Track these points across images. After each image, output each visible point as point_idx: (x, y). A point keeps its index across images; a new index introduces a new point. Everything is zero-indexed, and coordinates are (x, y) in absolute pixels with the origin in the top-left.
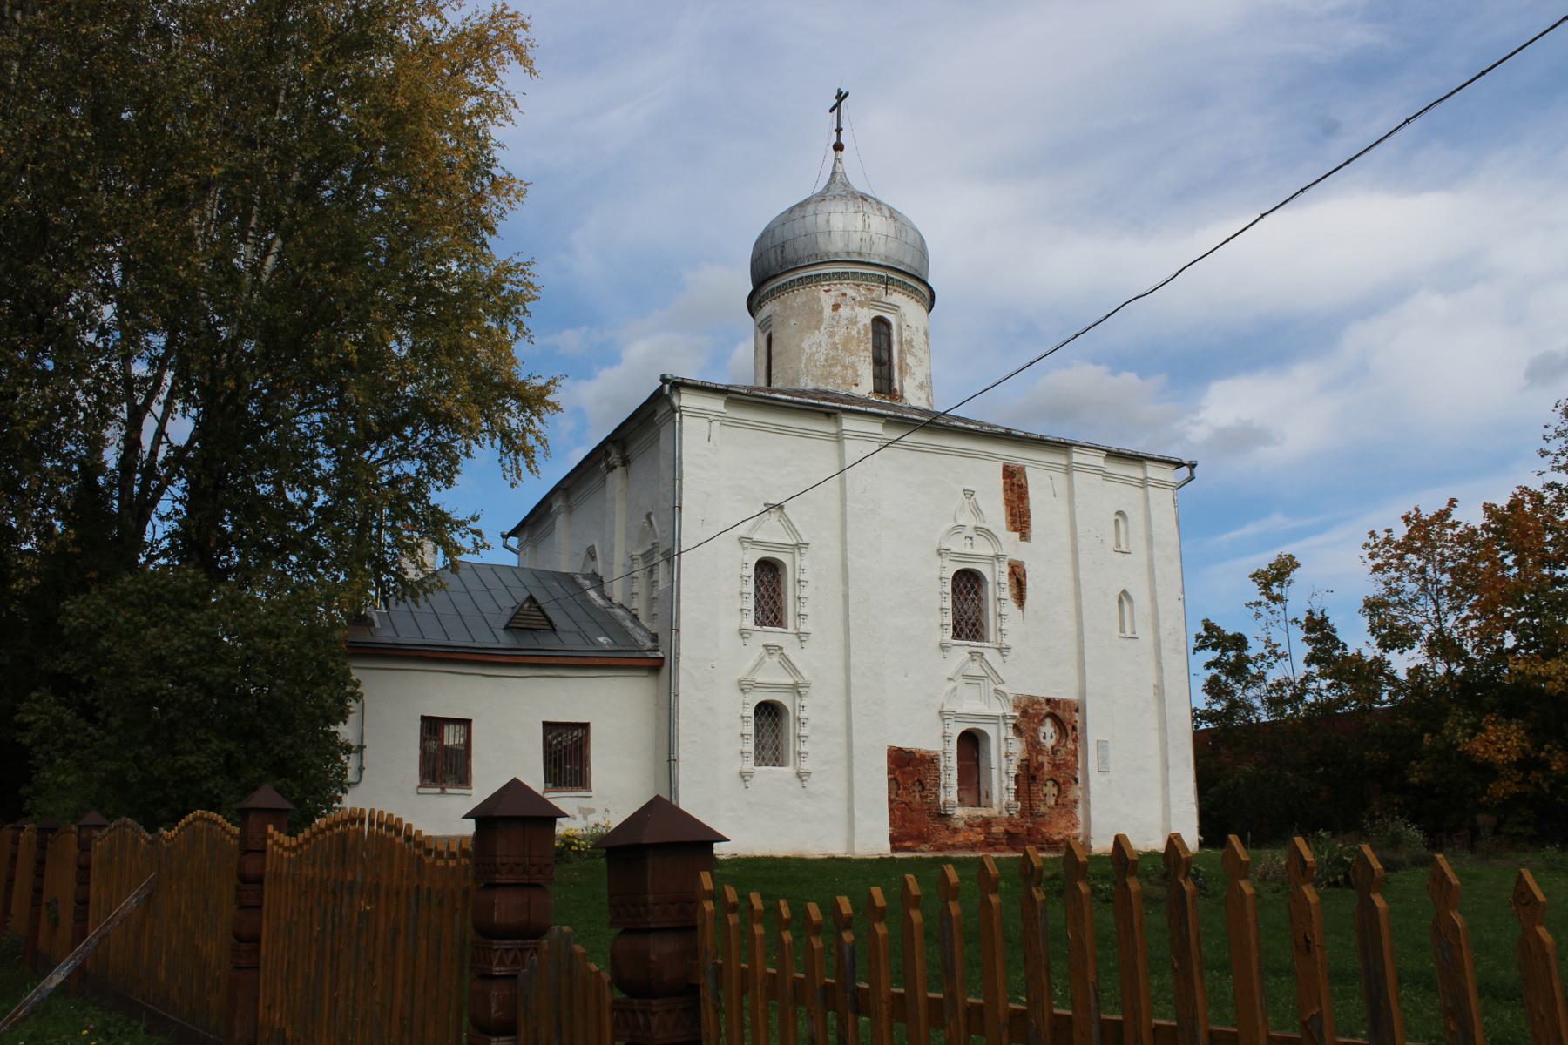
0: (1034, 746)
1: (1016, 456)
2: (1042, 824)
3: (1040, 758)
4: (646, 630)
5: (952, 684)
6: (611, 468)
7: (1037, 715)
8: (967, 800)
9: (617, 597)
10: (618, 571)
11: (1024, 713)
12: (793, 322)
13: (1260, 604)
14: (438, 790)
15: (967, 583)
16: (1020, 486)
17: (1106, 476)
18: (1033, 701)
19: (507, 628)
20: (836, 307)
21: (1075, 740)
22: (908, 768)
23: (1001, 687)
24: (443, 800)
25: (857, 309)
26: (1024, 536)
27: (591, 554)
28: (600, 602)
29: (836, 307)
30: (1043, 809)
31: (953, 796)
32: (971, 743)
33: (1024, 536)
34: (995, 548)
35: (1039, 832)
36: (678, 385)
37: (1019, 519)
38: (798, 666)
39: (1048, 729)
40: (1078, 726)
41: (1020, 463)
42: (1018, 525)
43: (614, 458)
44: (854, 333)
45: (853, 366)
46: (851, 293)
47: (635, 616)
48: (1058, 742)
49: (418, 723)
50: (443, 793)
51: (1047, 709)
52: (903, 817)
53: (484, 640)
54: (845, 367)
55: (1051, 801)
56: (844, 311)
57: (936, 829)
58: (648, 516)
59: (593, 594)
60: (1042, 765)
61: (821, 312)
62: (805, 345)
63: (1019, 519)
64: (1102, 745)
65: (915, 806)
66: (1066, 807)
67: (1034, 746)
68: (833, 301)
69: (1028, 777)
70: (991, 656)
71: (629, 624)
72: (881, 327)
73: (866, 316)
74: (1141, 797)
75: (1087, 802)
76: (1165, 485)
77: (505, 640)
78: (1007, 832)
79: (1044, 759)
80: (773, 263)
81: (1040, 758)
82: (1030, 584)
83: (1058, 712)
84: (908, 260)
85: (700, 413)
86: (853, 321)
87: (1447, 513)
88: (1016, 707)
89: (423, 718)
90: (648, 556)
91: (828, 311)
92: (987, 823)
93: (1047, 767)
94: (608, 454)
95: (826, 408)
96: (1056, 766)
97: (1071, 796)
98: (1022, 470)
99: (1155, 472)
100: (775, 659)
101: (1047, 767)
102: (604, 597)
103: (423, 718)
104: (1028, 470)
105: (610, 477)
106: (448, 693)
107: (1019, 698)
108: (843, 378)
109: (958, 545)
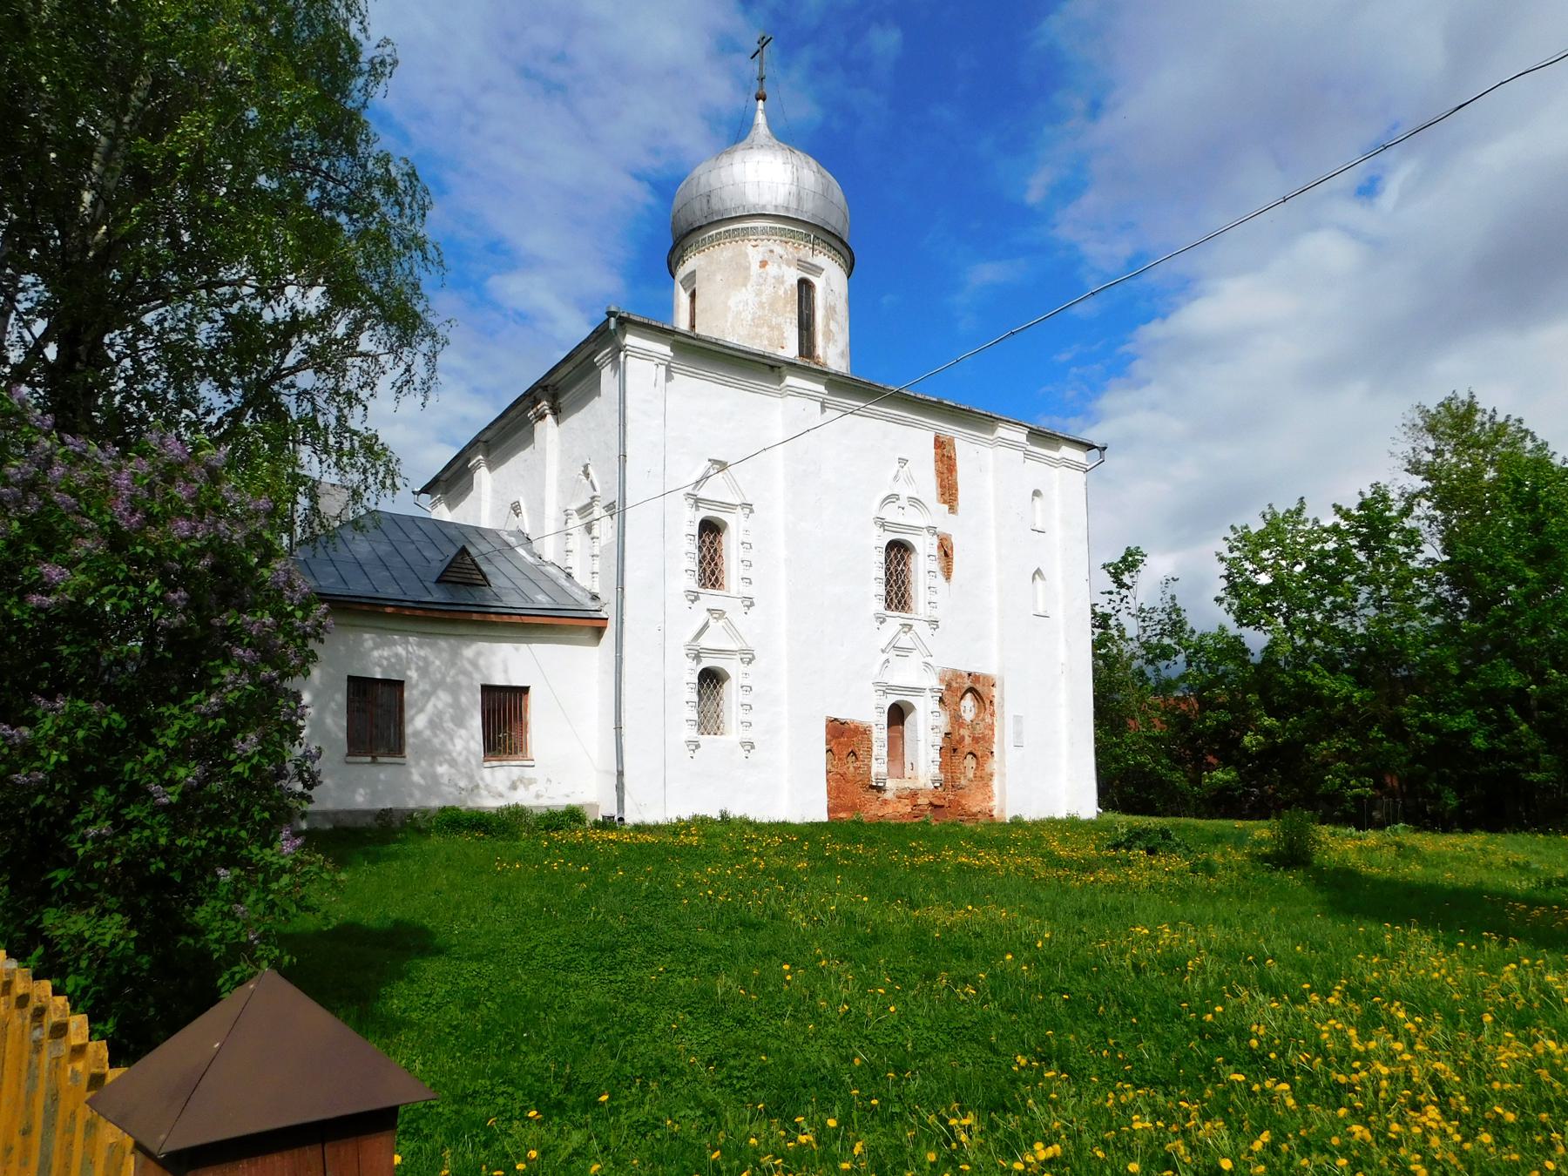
0: (956, 719)
1: (949, 430)
2: (962, 796)
3: (962, 732)
4: (584, 590)
5: (885, 656)
6: (542, 417)
7: (959, 689)
8: (893, 771)
9: (549, 556)
10: (551, 523)
11: (949, 686)
12: (719, 277)
13: (1111, 593)
14: (369, 759)
15: (898, 550)
16: (950, 458)
17: (1028, 455)
18: (957, 675)
19: (439, 581)
20: (763, 264)
21: (992, 715)
22: (844, 738)
23: (929, 660)
24: (374, 769)
25: (784, 267)
26: (952, 510)
27: (516, 508)
28: (530, 559)
29: (763, 264)
30: (963, 782)
31: (884, 769)
32: (898, 715)
33: (952, 510)
34: (921, 522)
35: (959, 804)
36: (624, 323)
37: (948, 492)
38: (741, 630)
39: (968, 702)
40: (996, 701)
41: (950, 434)
42: (947, 497)
43: (544, 405)
44: (781, 292)
45: (779, 327)
46: (778, 249)
47: (569, 575)
48: (977, 715)
49: (345, 685)
50: (374, 761)
51: (968, 684)
52: (838, 788)
53: (416, 593)
54: (772, 328)
55: (971, 775)
56: (772, 269)
57: (869, 801)
58: (586, 467)
59: (521, 551)
60: (963, 738)
61: (748, 268)
62: (731, 303)
63: (948, 492)
64: (1018, 719)
65: (850, 777)
66: (984, 779)
67: (956, 719)
68: (760, 258)
69: (951, 748)
70: (921, 628)
71: (563, 582)
72: (805, 287)
73: (793, 276)
74: (1048, 771)
75: (1004, 775)
76: (1077, 466)
77: (438, 595)
78: (931, 804)
79: (965, 732)
80: (698, 213)
81: (962, 732)
82: (957, 556)
83: (978, 687)
84: (833, 222)
85: (646, 355)
86: (780, 280)
87: (1299, 512)
88: (942, 680)
89: (350, 679)
90: (585, 510)
91: (755, 267)
92: (914, 794)
93: (968, 740)
94: (536, 402)
95: (758, 367)
96: (976, 740)
97: (988, 769)
98: (952, 440)
99: (1067, 452)
100: (721, 622)
101: (968, 740)
102: (533, 555)
103: (350, 679)
104: (957, 442)
105: (539, 426)
106: (383, 653)
107: (944, 671)
108: (770, 340)
109: (891, 514)
